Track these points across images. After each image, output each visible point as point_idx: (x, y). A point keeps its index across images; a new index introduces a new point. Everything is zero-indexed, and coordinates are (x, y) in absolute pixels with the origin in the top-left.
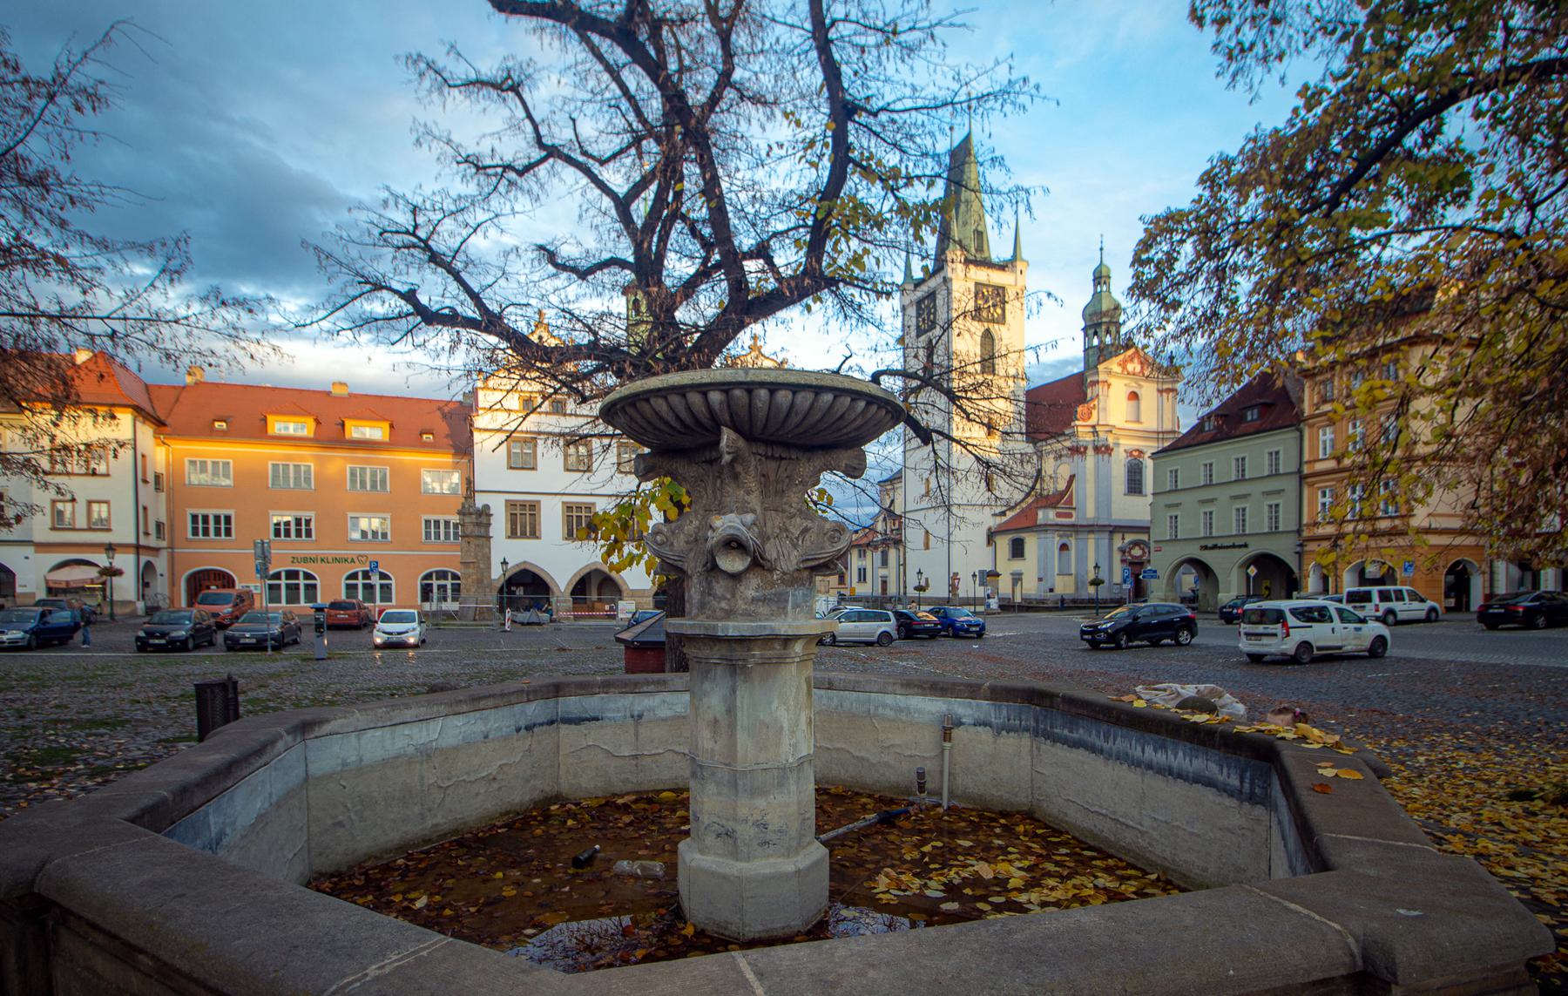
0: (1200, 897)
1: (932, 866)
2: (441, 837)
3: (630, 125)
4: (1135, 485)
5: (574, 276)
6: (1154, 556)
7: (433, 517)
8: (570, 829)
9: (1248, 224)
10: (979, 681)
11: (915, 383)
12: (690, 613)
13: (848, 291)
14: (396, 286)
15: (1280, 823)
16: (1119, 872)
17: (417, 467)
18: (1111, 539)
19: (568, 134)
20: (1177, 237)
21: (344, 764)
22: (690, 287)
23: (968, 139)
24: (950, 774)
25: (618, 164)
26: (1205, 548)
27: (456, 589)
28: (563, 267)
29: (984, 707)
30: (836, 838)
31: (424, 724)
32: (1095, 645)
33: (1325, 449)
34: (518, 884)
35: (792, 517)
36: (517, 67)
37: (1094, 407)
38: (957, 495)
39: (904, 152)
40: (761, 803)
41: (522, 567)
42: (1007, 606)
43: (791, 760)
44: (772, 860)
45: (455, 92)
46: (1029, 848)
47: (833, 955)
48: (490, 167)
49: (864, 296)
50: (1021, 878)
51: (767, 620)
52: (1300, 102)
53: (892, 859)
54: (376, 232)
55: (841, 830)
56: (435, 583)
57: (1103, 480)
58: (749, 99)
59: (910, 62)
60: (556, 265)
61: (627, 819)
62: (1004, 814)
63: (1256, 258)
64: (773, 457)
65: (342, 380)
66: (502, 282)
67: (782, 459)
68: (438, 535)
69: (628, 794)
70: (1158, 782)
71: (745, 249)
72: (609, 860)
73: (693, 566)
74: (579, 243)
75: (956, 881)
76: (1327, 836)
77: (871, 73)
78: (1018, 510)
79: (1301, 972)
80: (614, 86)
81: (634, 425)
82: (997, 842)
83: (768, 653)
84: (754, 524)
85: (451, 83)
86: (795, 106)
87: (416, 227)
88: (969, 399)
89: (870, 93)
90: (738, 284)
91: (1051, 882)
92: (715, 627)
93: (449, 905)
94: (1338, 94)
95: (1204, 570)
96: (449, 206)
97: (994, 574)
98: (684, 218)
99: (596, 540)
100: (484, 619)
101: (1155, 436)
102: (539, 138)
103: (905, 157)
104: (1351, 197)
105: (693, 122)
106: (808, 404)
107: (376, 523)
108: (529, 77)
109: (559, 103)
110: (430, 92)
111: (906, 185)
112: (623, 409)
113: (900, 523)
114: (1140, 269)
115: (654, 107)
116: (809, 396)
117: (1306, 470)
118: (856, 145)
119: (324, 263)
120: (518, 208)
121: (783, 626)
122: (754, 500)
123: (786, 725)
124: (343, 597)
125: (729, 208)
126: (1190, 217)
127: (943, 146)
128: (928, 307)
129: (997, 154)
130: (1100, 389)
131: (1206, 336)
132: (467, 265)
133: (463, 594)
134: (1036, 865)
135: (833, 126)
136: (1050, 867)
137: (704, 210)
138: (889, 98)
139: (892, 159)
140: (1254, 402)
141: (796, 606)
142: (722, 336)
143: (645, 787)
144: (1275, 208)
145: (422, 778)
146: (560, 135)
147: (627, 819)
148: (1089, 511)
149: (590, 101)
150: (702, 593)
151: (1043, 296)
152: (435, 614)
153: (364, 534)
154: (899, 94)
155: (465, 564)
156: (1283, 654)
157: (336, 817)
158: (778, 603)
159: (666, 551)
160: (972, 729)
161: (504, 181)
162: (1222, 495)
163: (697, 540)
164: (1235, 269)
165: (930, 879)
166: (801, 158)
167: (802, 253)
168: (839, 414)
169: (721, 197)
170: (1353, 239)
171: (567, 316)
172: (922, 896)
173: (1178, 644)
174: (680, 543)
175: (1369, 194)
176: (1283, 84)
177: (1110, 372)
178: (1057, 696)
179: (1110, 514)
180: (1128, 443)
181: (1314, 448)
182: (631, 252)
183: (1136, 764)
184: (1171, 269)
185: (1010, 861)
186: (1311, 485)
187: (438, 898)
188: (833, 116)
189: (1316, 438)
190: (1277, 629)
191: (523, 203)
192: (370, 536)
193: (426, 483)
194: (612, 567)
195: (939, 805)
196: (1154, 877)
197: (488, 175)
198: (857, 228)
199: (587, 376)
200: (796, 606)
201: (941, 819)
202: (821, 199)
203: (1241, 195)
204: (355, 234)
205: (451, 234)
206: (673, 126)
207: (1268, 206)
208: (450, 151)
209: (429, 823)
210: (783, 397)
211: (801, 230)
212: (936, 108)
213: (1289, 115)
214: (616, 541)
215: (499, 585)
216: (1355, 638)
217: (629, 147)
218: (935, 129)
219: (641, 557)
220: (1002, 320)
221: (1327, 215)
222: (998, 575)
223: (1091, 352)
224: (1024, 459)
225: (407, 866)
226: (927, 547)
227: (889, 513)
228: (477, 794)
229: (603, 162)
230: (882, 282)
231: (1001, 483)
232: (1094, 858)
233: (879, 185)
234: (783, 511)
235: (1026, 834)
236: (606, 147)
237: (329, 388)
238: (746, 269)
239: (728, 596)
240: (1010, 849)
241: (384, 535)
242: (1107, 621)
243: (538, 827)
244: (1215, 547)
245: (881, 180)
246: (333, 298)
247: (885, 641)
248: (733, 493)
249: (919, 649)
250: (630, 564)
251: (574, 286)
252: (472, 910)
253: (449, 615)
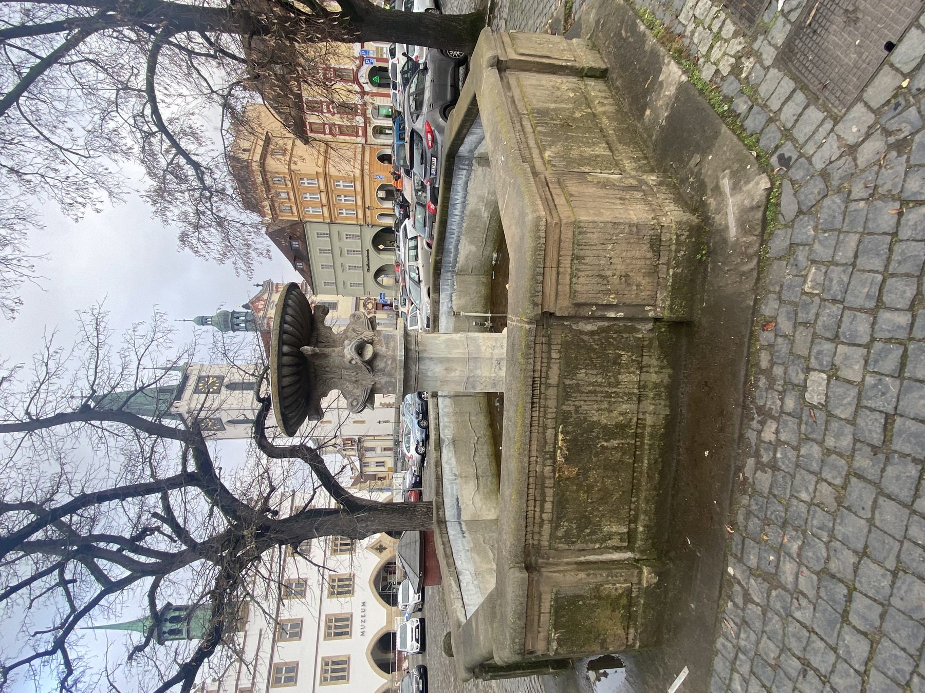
26: (368, 270)
80: (20, 592)
95: (380, 272)
102: (47, 653)
146: (46, 642)
162: (339, 261)
181: (317, 217)
189: (311, 216)
210: (288, 318)
223: (248, 328)
244: (368, 265)
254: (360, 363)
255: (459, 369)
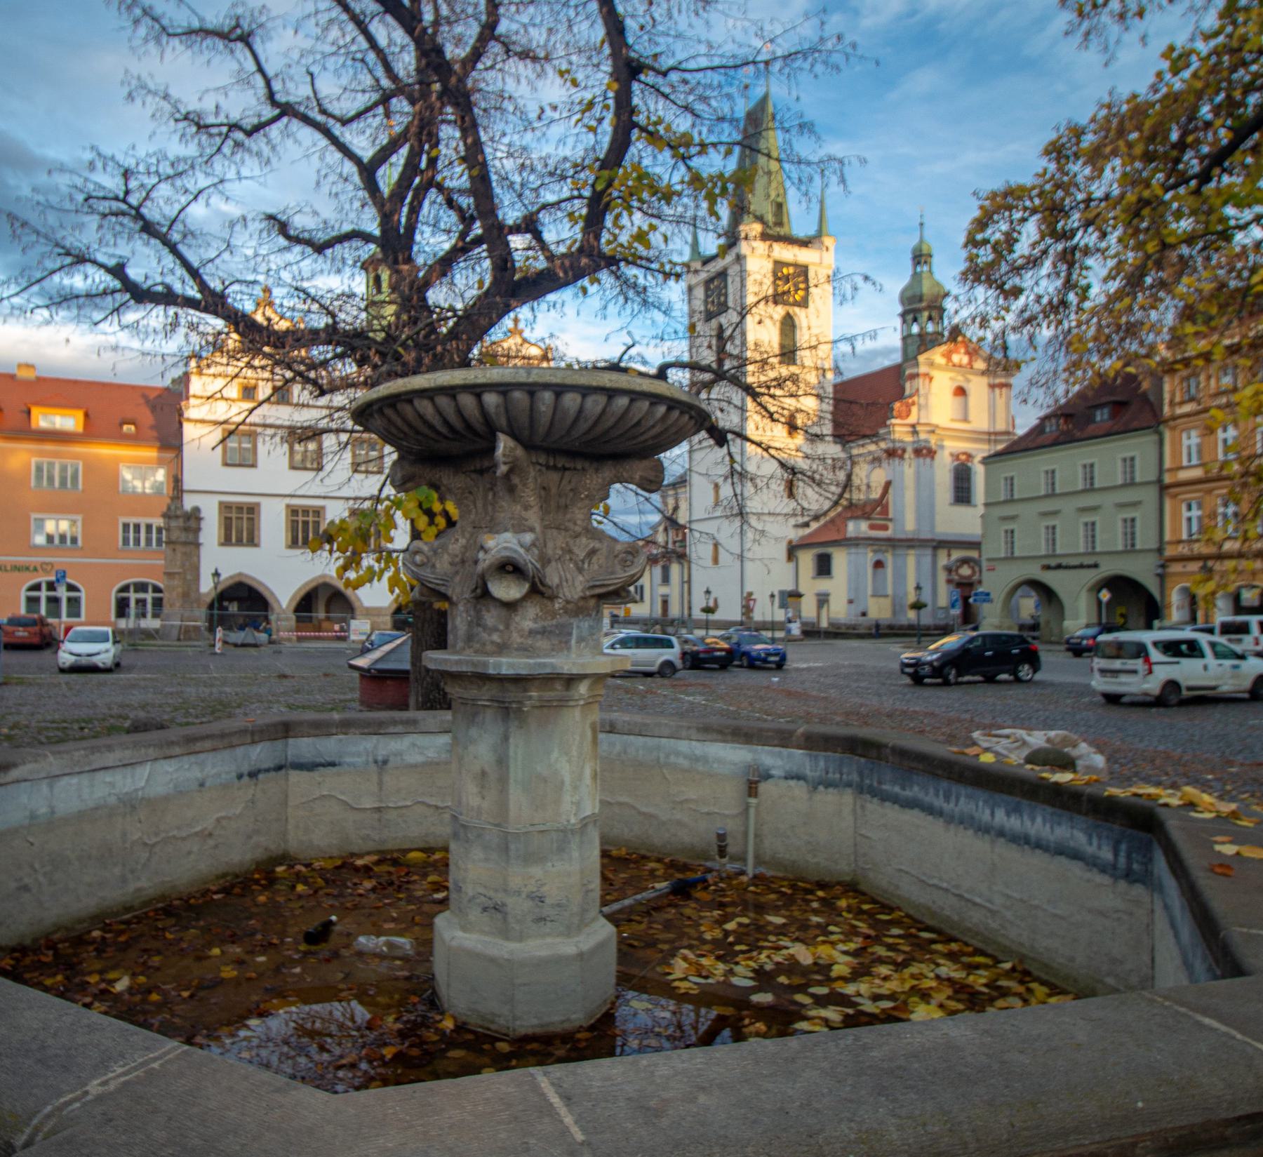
0: (1091, 1005)
1: (738, 948)
2: (146, 904)
3: (377, 80)
4: (962, 494)
5: (309, 250)
6: (986, 576)
7: (132, 520)
8: (300, 897)
9: (1101, 200)
10: (791, 727)
11: (707, 376)
12: (454, 646)
13: (631, 272)
14: (101, 258)
15: (1166, 907)
16: (965, 959)
17: (117, 461)
18: (934, 556)
19: (306, 91)
20: (1017, 215)
21: (33, 816)
22: (445, 264)
23: (765, 99)
24: (756, 836)
25: (362, 125)
26: (1047, 567)
27: (158, 603)
28: (297, 240)
29: (798, 758)
30: (620, 911)
31: (129, 769)
32: (918, 679)
33: (1189, 455)
34: (240, 963)
35: (577, 536)
36: (248, 14)
37: (913, 404)
38: (753, 505)
39: (697, 116)
40: (536, 871)
41: (237, 579)
42: (811, 632)
43: (573, 821)
44: (549, 940)
45: (176, 41)
46: (855, 927)
47: (652, 1072)
48: (213, 126)
49: (650, 278)
50: (846, 964)
51: (546, 656)
52: (1165, 65)
53: (690, 938)
54: (80, 198)
55: (627, 902)
56: (133, 596)
57: (924, 486)
58: (516, 54)
59: (705, 15)
60: (288, 237)
61: (368, 884)
62: (822, 885)
63: (1113, 238)
64: (555, 468)
65: (30, 362)
66: (226, 256)
67: (565, 469)
68: (137, 542)
69: (369, 853)
70: (1011, 853)
71: (510, 222)
72: (349, 935)
73: (460, 591)
74: (315, 213)
75: (769, 967)
76: (1236, 932)
77: (660, 28)
78: (822, 521)
79: (1225, 1105)
80: (361, 39)
81: (394, 430)
82: (816, 919)
83: (548, 695)
84: (533, 544)
85: (171, 31)
86: (571, 63)
87: (127, 192)
88: (773, 396)
89: (658, 50)
90: (503, 263)
91: (884, 970)
92: (485, 664)
93: (156, 988)
94: (1209, 55)
95: (1047, 594)
96: (166, 169)
97: (796, 595)
98: (440, 188)
99: (331, 552)
100: (190, 639)
101: (986, 437)
102: (271, 96)
103: (698, 121)
104: (1224, 170)
105: (453, 80)
106: (599, 408)
107: (64, 526)
108: (261, 26)
109: (295, 55)
110: (146, 40)
111: (700, 153)
112: (381, 411)
113: (684, 534)
114: (975, 251)
115: (406, 62)
116: (602, 400)
117: (1168, 479)
118: (643, 108)
119: (19, 231)
120: (245, 172)
121: (566, 663)
122: (533, 517)
123: (567, 779)
124: (23, 611)
125: (494, 177)
126: (1034, 192)
127: (741, 108)
128: (717, 287)
129: (806, 120)
130: (920, 382)
131: (1053, 327)
132: (185, 236)
133: (166, 609)
134: (864, 949)
135: (616, 86)
136: (881, 951)
137: (465, 177)
138: (680, 56)
139: (682, 124)
140: (1104, 400)
141: (581, 639)
142: (484, 322)
143: (389, 846)
144: (1134, 183)
145: (124, 834)
146: (297, 92)
147: (368, 884)
148: (907, 522)
149: (333, 54)
150: (470, 624)
151: (859, 281)
152: (131, 632)
153: (50, 538)
154: (692, 52)
155: (169, 575)
156: (1146, 694)
157: (21, 879)
158: (560, 636)
159: (426, 573)
160: (783, 783)
161: (230, 143)
163: (465, 561)
164: (1086, 251)
165: (737, 963)
166: (578, 121)
167: (578, 228)
168: (635, 420)
169: (484, 165)
170: (1228, 219)
171: (302, 295)
172: (726, 983)
173: (1018, 680)
174: (443, 564)
175: (1245, 166)
176: (1145, 44)
177: (931, 364)
178: (886, 746)
179: (933, 526)
180: (954, 445)
181: (1176, 454)
182: (376, 224)
183: (984, 830)
184: (1011, 251)
185: (833, 944)
186: (1174, 496)
187: (142, 979)
188: (615, 75)
190: (1138, 664)
191: (251, 167)
192: (57, 541)
193: (125, 481)
194: (348, 583)
195: (743, 873)
196: (1008, 966)
197: (211, 135)
198: (641, 200)
199: (324, 364)
200: (581, 639)
201: (745, 889)
202: (601, 168)
203: (1094, 169)
204: (54, 200)
205: (168, 200)
206: (429, 85)
207: (1129, 180)
208: (167, 107)
209: (131, 887)
211: (576, 201)
212: (735, 67)
213: (1151, 79)
214: (354, 553)
215: (209, 600)
216: (1232, 677)
217: (376, 105)
218: (733, 90)
219: (382, 572)
220: (804, 303)
221: (1197, 192)
222: (799, 596)
223: (909, 341)
224: (836, 465)
225: (103, 938)
226: (716, 560)
227: (671, 522)
228: (189, 853)
229: (345, 122)
230: (670, 262)
231: (809, 492)
232: (933, 942)
233: (667, 153)
234: (566, 530)
235: (849, 909)
236: (348, 106)
237: (15, 371)
238: (512, 245)
239: (501, 627)
240: (832, 928)
241: (74, 540)
242: (933, 650)
243: (261, 893)
244: (1059, 567)
245: (671, 147)
246: (27, 272)
247: (668, 671)
248: (508, 509)
249: (707, 681)
250: (370, 581)
251: (307, 262)
252: (185, 994)
253: (148, 634)
254: (481, 567)
255: (485, 805)
